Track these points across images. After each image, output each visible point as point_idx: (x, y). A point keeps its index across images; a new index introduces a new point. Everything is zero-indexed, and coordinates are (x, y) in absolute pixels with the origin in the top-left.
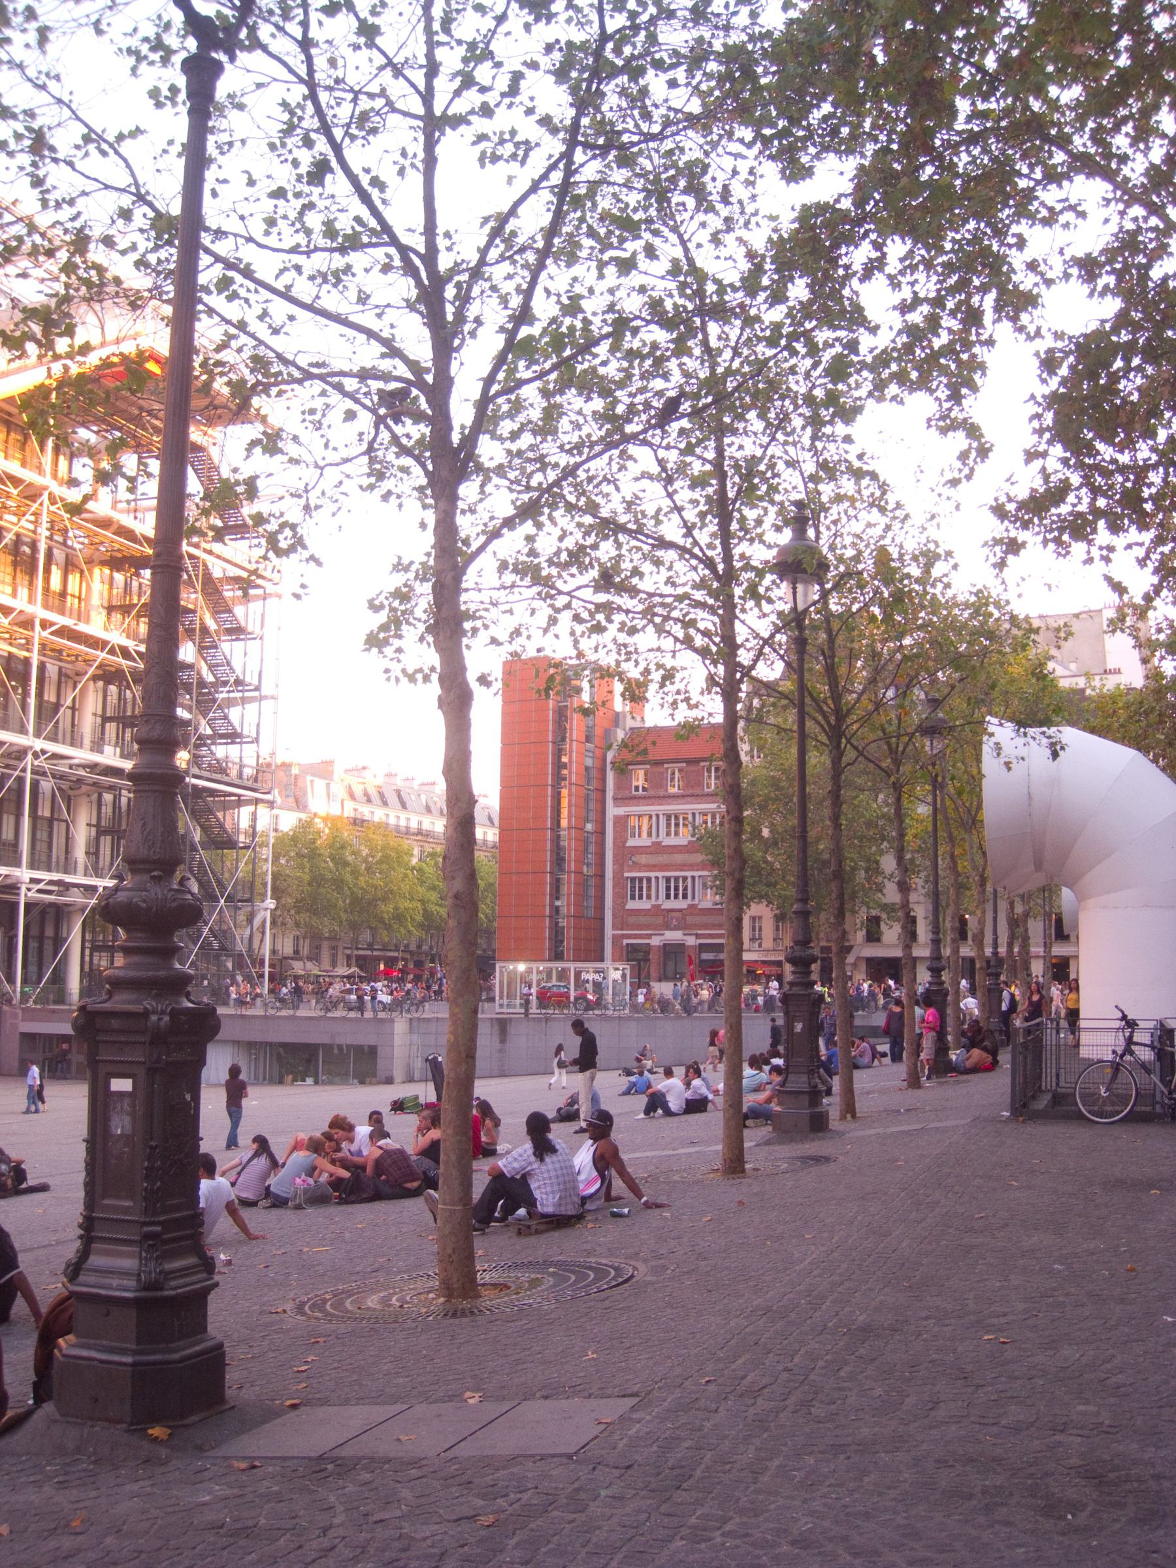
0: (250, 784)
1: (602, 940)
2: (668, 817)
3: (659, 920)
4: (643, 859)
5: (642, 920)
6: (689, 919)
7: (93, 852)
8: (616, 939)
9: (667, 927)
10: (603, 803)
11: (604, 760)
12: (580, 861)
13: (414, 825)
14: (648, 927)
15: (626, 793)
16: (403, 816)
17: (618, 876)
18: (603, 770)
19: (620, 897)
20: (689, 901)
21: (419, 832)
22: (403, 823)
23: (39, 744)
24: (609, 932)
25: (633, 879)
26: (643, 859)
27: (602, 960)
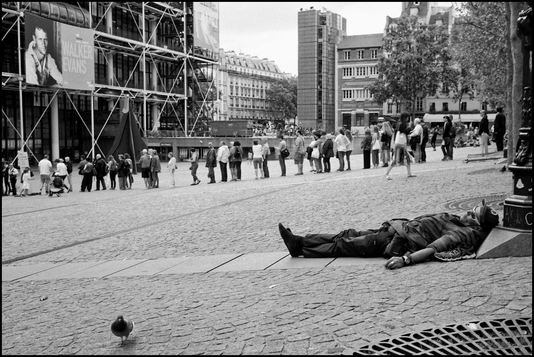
0: (210, 58)
1: (334, 113)
2: (358, 68)
3: (355, 105)
4: (348, 84)
5: (348, 105)
6: (366, 105)
7: (159, 83)
8: (339, 112)
9: (357, 107)
10: (334, 63)
11: (334, 48)
12: (327, 85)
13: (250, 72)
14: (350, 108)
15: (342, 60)
16: (247, 69)
17: (340, 90)
18: (334, 52)
19: (340, 97)
20: (366, 98)
21: (253, 75)
22: (247, 72)
23: (147, 45)
24: (337, 109)
25: (345, 91)
26: (348, 84)
27: (100, 99)
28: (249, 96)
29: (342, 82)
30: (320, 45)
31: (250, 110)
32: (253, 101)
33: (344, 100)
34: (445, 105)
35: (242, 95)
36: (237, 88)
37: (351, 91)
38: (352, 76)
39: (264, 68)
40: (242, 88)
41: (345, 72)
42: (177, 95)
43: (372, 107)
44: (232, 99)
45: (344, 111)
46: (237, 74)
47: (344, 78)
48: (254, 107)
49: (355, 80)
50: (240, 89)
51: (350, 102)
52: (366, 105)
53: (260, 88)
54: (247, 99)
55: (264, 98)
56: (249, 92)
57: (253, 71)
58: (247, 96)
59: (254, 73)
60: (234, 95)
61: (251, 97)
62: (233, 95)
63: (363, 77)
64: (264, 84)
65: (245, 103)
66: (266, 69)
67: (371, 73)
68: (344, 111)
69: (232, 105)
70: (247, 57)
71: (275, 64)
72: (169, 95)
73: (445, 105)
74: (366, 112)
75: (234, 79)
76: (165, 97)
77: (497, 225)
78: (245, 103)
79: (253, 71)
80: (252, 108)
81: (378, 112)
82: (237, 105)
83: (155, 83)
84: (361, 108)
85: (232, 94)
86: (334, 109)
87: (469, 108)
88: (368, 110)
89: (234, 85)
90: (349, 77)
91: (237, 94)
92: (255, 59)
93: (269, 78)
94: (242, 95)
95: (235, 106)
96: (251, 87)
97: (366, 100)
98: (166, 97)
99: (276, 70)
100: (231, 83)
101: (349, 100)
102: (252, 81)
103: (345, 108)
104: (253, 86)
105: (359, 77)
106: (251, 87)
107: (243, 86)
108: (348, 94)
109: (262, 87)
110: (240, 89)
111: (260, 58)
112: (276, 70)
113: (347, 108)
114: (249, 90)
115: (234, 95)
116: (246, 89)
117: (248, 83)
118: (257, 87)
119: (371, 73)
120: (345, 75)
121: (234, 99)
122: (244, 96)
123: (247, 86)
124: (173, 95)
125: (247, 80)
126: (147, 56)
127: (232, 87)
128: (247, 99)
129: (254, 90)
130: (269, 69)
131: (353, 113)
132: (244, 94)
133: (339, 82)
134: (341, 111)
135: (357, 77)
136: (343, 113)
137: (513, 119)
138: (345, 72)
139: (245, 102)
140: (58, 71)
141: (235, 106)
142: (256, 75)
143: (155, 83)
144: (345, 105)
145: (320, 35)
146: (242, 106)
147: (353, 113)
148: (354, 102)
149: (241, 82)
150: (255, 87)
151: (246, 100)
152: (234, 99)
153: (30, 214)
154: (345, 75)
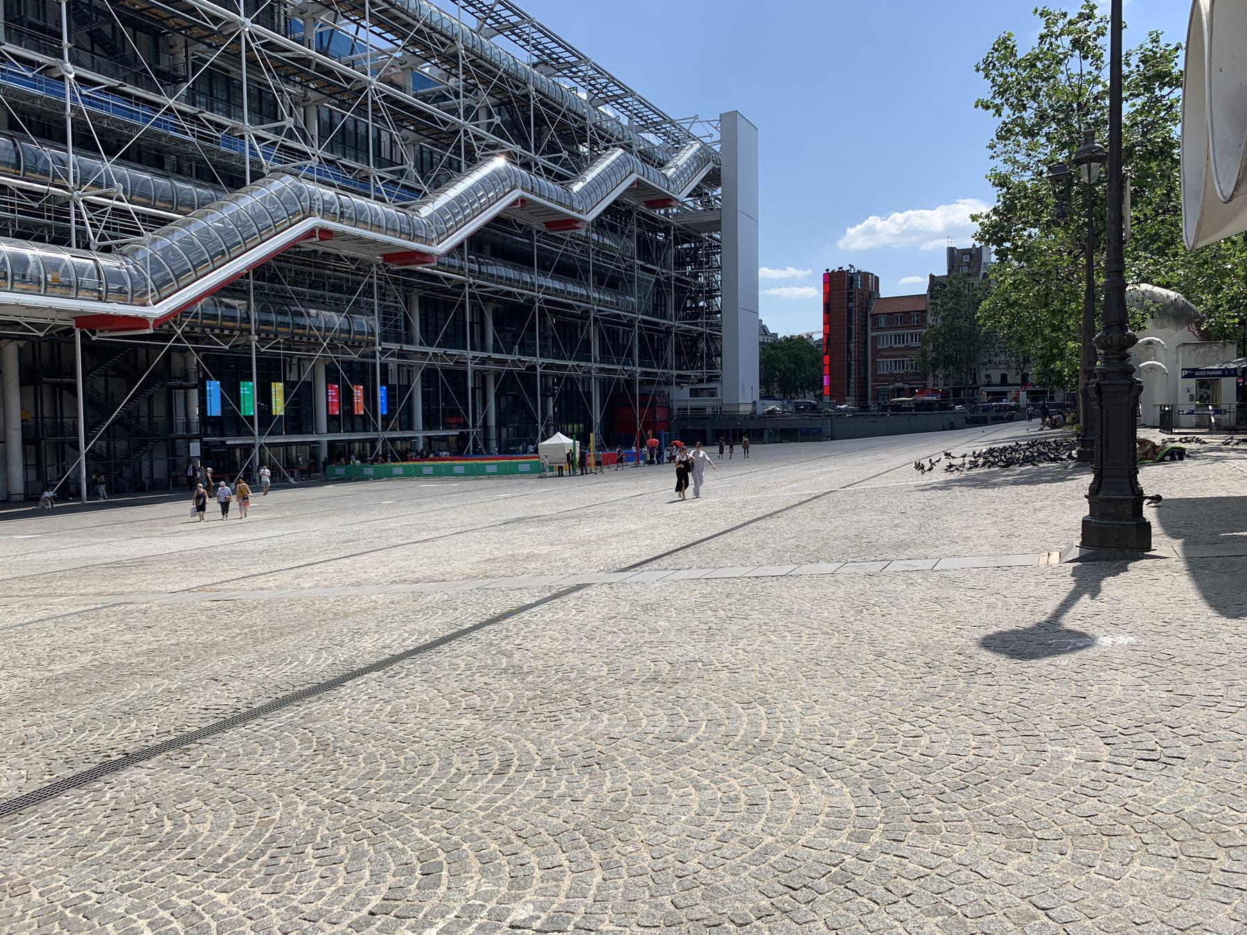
24: (870, 384)
30: (850, 312)
34: (1004, 377)
42: (523, 358)
63: (902, 345)
72: (570, 363)
73: (1004, 377)
76: (503, 362)
77: (1149, 549)
83: (490, 341)
86: (867, 383)
87: (1010, 380)
98: (427, 353)
124: (575, 363)
126: (472, 296)
137: (446, 505)
143: (490, 341)
145: (850, 300)
153: (242, 582)
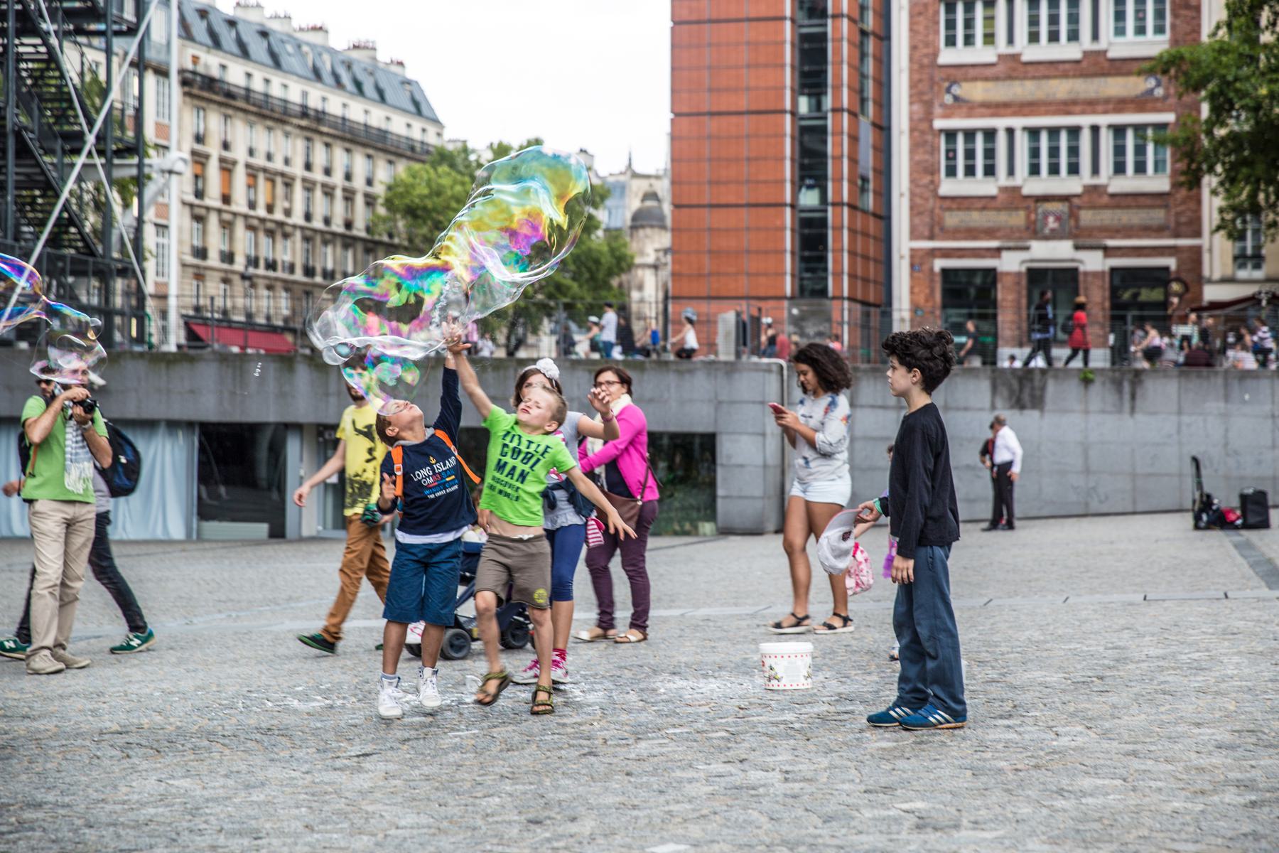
3: (1018, 219)
4: (976, 91)
5: (976, 218)
6: (1087, 217)
8: (919, 261)
9: (1035, 231)
13: (294, 96)
14: (990, 233)
16: (277, 80)
19: (924, 171)
24: (903, 244)
25: (951, 135)
26: (976, 91)
28: (288, 213)
29: (934, 81)
31: (288, 286)
32: (307, 239)
33: (948, 187)
35: (252, 205)
36: (227, 167)
37: (990, 134)
38: (1001, 45)
39: (358, 84)
40: (252, 172)
41: (951, 25)
43: (1127, 231)
44: (199, 219)
45: (947, 253)
46: (229, 95)
47: (947, 56)
48: (309, 271)
49: (1014, 68)
50: (240, 176)
51: (985, 203)
52: (1087, 217)
53: (337, 179)
54: (277, 231)
55: (359, 230)
56: (289, 197)
57: (305, 94)
58: (278, 216)
59: (314, 102)
60: (213, 199)
61: (297, 218)
62: (208, 202)
63: (1067, 51)
64: (360, 165)
65: (266, 249)
66: (369, 88)
67: (1120, 31)
68: (947, 253)
69: (201, 253)
70: (274, 26)
71: (410, 74)
74: (1093, 262)
75: (214, 122)
78: (266, 249)
79: (305, 94)
80: (299, 276)
81: (1171, 262)
82: (228, 257)
84: (1054, 236)
85: (199, 194)
88: (1108, 252)
89: (213, 149)
90: (981, 54)
91: (226, 199)
92: (315, 38)
93: (383, 134)
94: (252, 205)
95: (214, 260)
96: (297, 170)
97: (1092, 190)
99: (416, 104)
100: (199, 139)
101: (981, 186)
102: (300, 144)
103: (955, 234)
104: (308, 167)
105: (1044, 51)
106: (297, 170)
107: (259, 161)
108: (979, 151)
109: (348, 177)
110: (240, 176)
111: (339, 41)
112: (416, 104)
113: (972, 233)
114: (288, 185)
115: (213, 199)
116: (271, 176)
117: (284, 148)
118: (328, 172)
119: (1120, 31)
120: (951, 41)
121: (213, 220)
122: (261, 212)
123: (278, 165)
125: (279, 134)
127: (199, 159)
128: (277, 231)
129: (309, 186)
130: (381, 92)
131: (1011, 263)
132: (262, 201)
133: (913, 85)
134: (933, 253)
135: (1031, 53)
136: (939, 264)
138: (951, 25)
139: (264, 241)
140: (449, 663)
141: (214, 260)
142: (320, 116)
144: (952, 219)
146: (253, 262)
147: (1011, 263)
148: (1013, 198)
149: (247, 139)
150: (318, 176)
151: (270, 233)
152: (213, 220)
154: (951, 41)
